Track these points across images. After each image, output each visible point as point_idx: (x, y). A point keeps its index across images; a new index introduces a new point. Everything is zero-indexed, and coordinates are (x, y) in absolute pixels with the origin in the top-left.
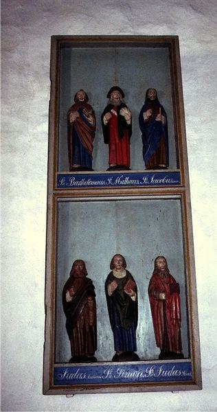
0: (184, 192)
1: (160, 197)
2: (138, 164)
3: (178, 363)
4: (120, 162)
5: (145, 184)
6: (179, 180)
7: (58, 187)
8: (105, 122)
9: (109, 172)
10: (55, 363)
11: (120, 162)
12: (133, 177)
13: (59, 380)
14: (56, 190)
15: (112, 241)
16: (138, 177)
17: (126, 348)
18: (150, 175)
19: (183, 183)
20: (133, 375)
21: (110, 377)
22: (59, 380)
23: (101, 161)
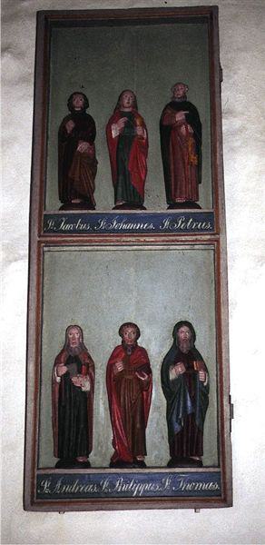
0: (218, 241)
1: (180, 258)
2: (156, 202)
3: (197, 467)
4: (130, 196)
5: (166, 231)
6: (210, 224)
7: (45, 232)
8: (114, 134)
9: (61, 212)
10: (38, 469)
11: (130, 196)
12: (197, 218)
13: (45, 492)
14: (43, 236)
15: (134, 295)
16: (157, 219)
17: (130, 451)
18: (174, 219)
19: (39, 503)
20: (139, 489)
21: (106, 490)
22: (45, 492)
23: (156, 202)
